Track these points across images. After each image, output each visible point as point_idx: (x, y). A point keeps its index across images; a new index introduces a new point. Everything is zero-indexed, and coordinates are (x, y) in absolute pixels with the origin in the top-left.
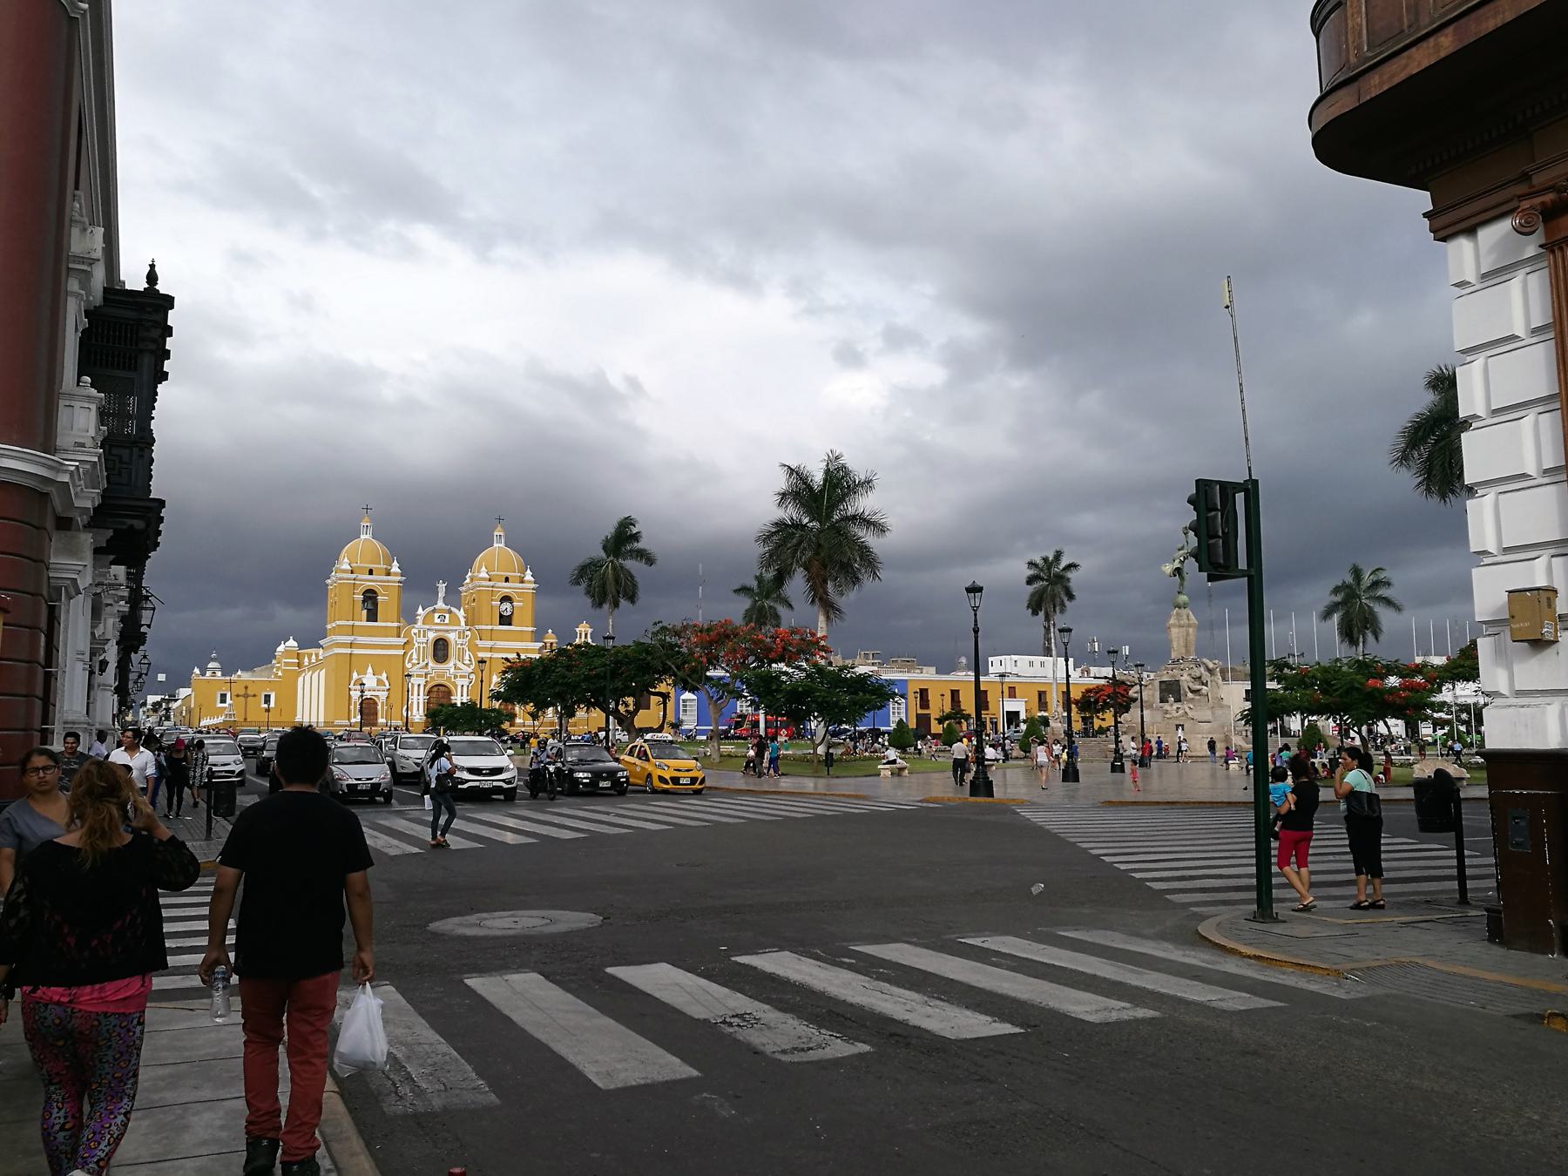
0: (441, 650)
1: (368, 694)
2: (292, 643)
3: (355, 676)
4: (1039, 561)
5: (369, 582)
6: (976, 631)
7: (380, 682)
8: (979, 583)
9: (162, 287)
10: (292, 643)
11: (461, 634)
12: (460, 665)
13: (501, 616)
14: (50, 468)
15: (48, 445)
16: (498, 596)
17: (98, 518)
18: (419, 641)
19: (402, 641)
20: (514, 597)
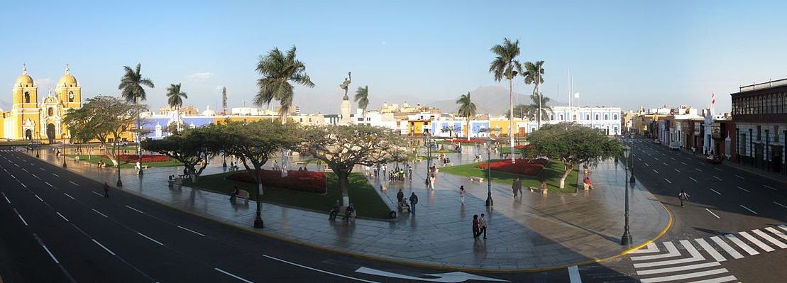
0: (50, 111)
18: (44, 109)
19: (39, 109)
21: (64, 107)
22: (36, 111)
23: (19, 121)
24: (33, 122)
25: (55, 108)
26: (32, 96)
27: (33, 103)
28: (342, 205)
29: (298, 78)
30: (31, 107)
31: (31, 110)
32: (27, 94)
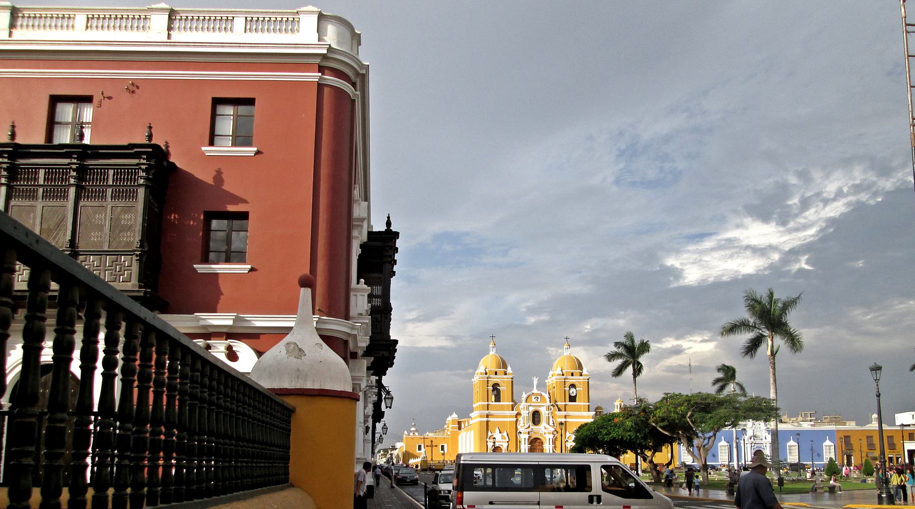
0: (536, 417)
1: (497, 444)
2: (455, 416)
3: (489, 434)
4: (613, 349)
5: (495, 379)
6: (878, 396)
7: (503, 437)
8: (879, 364)
9: (394, 228)
10: (455, 416)
11: (548, 409)
12: (547, 426)
13: (570, 396)
14: (349, 327)
15: (347, 317)
16: (567, 385)
17: (368, 353)
18: (525, 413)
19: (515, 412)
20: (577, 385)
21: (560, 410)
22: (510, 417)
23: (481, 433)
24: (505, 434)
25: (543, 411)
26: (504, 389)
27: (506, 402)
28: (372, 497)
29: (633, 341)
30: (502, 408)
31: (503, 414)
32: (496, 387)
